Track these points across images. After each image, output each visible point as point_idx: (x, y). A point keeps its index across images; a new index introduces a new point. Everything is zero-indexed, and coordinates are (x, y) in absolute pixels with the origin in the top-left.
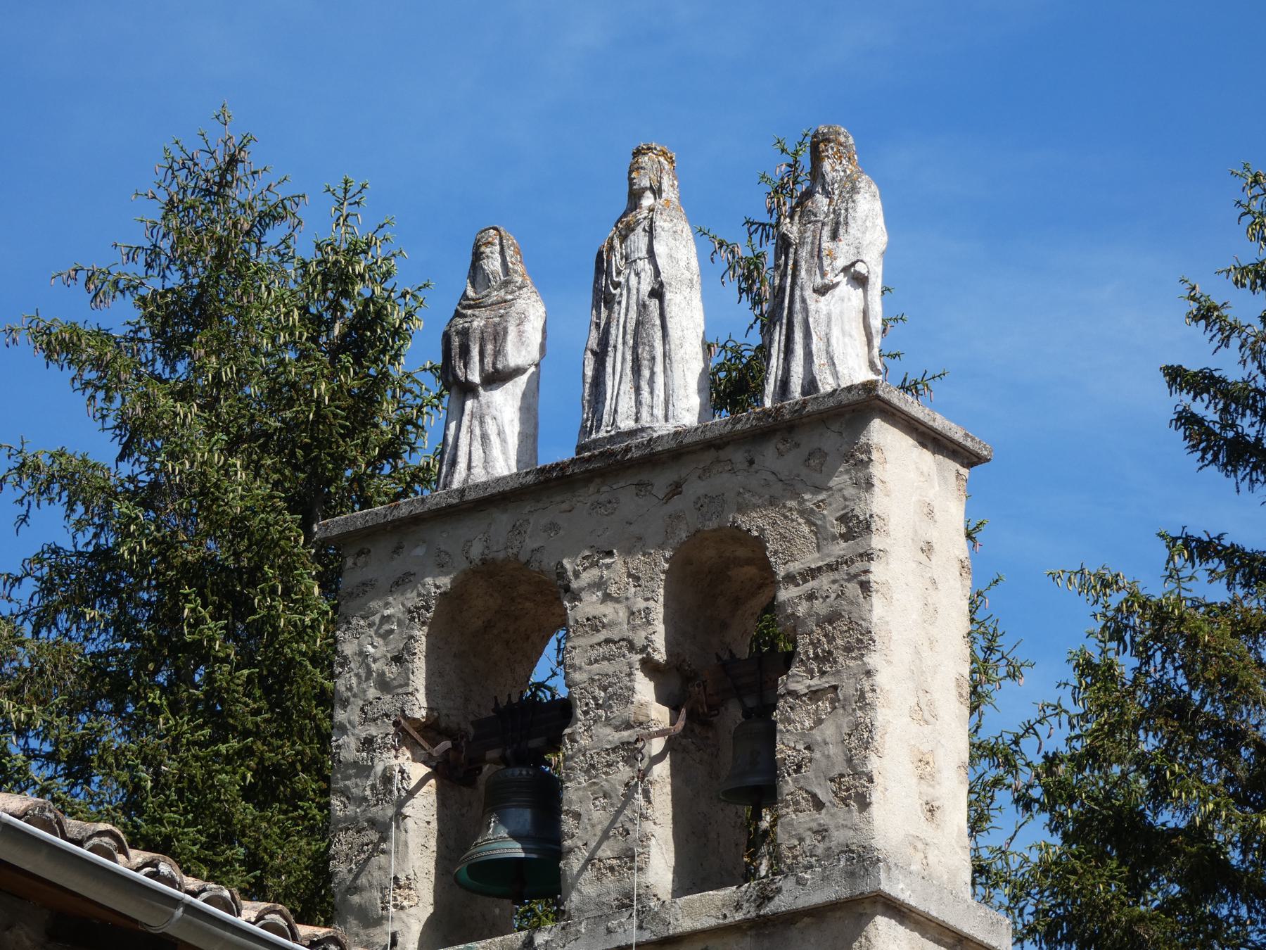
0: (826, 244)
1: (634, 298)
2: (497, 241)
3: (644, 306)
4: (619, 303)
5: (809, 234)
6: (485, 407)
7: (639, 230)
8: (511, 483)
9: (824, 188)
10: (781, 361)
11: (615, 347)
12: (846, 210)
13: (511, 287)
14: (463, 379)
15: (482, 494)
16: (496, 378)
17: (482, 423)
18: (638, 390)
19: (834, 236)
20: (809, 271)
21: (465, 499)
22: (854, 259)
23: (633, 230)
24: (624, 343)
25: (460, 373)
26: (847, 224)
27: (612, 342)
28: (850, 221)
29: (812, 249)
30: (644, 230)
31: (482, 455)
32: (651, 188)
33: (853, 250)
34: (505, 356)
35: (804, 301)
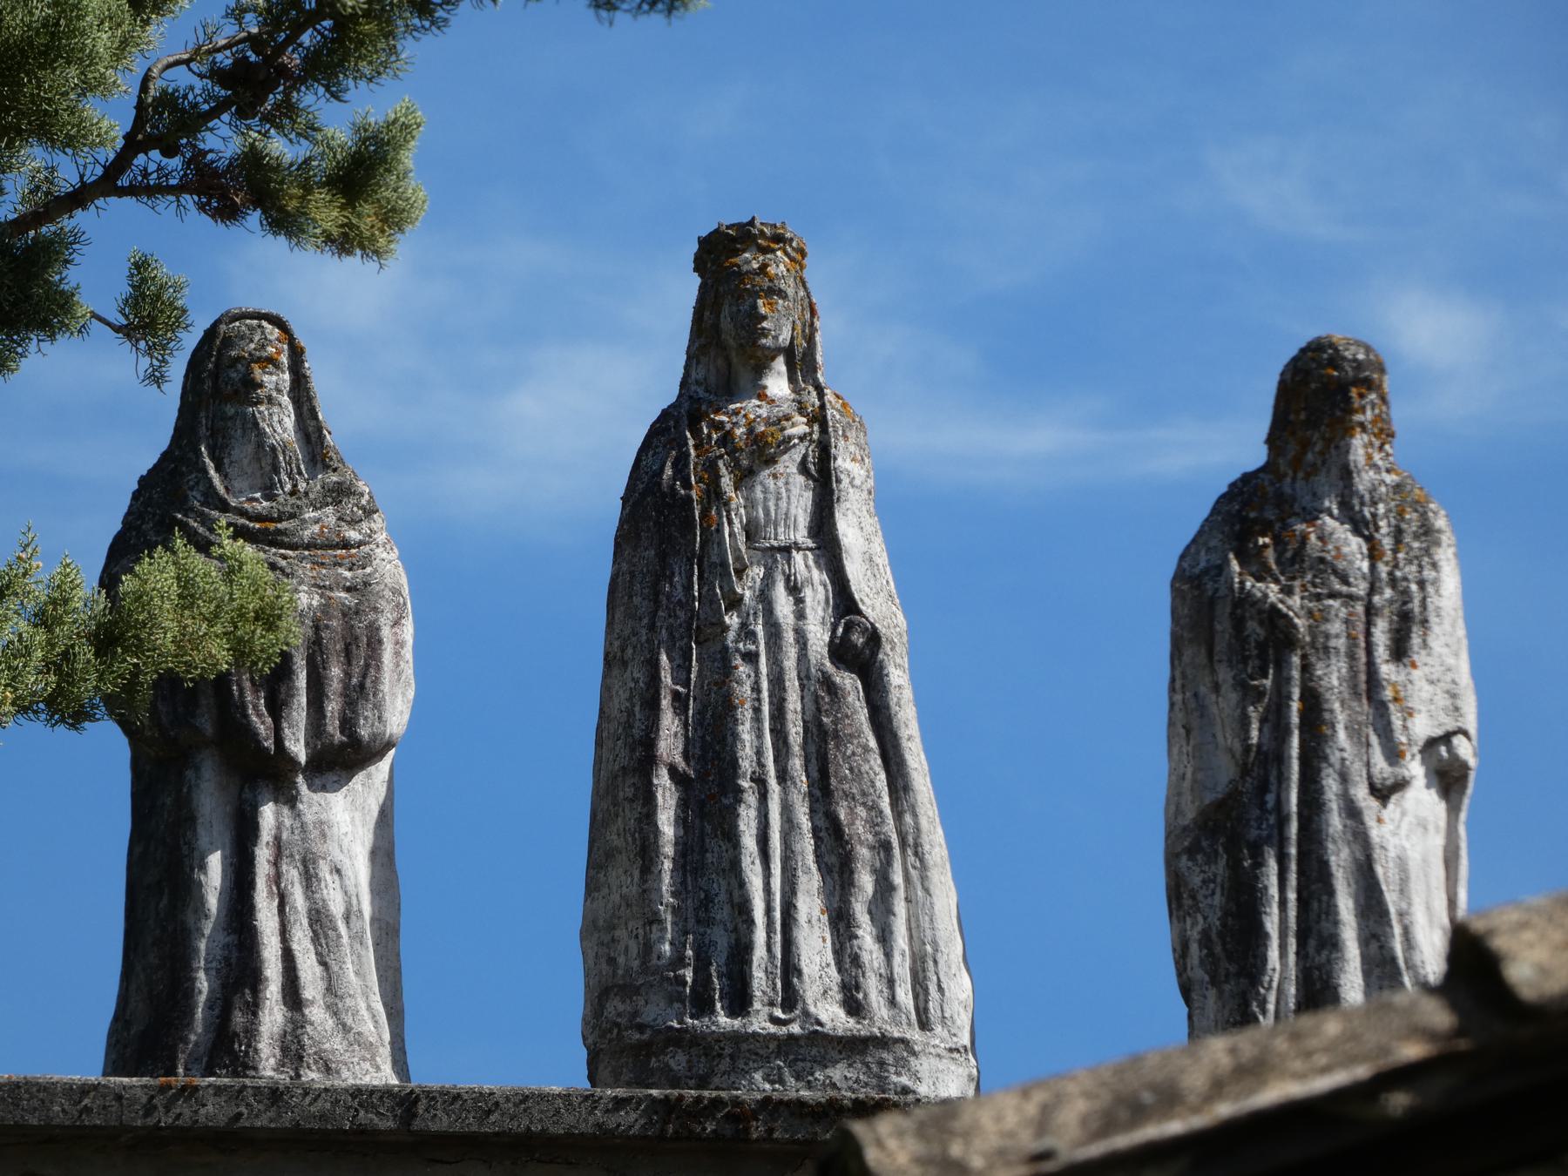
0: (1386, 670)
1: (790, 663)
2: (284, 359)
3: (828, 684)
4: (751, 658)
5: (1336, 627)
6: (314, 834)
7: (789, 464)
8: (569, 1119)
9: (1345, 505)
10: (1292, 958)
11: (760, 782)
12: (1422, 584)
13: (349, 506)
14: (269, 744)
15: (471, 1124)
16: (341, 759)
17: (310, 879)
18: (841, 922)
19: (1400, 651)
20: (1354, 732)
21: (417, 1125)
22: (1450, 725)
23: (771, 461)
24: (783, 776)
25: (262, 726)
26: (1425, 622)
27: (747, 765)
28: (1433, 619)
29: (1353, 670)
30: (803, 468)
31: (318, 969)
32: (789, 352)
33: (1442, 701)
34: (378, 707)
35: (1352, 812)
